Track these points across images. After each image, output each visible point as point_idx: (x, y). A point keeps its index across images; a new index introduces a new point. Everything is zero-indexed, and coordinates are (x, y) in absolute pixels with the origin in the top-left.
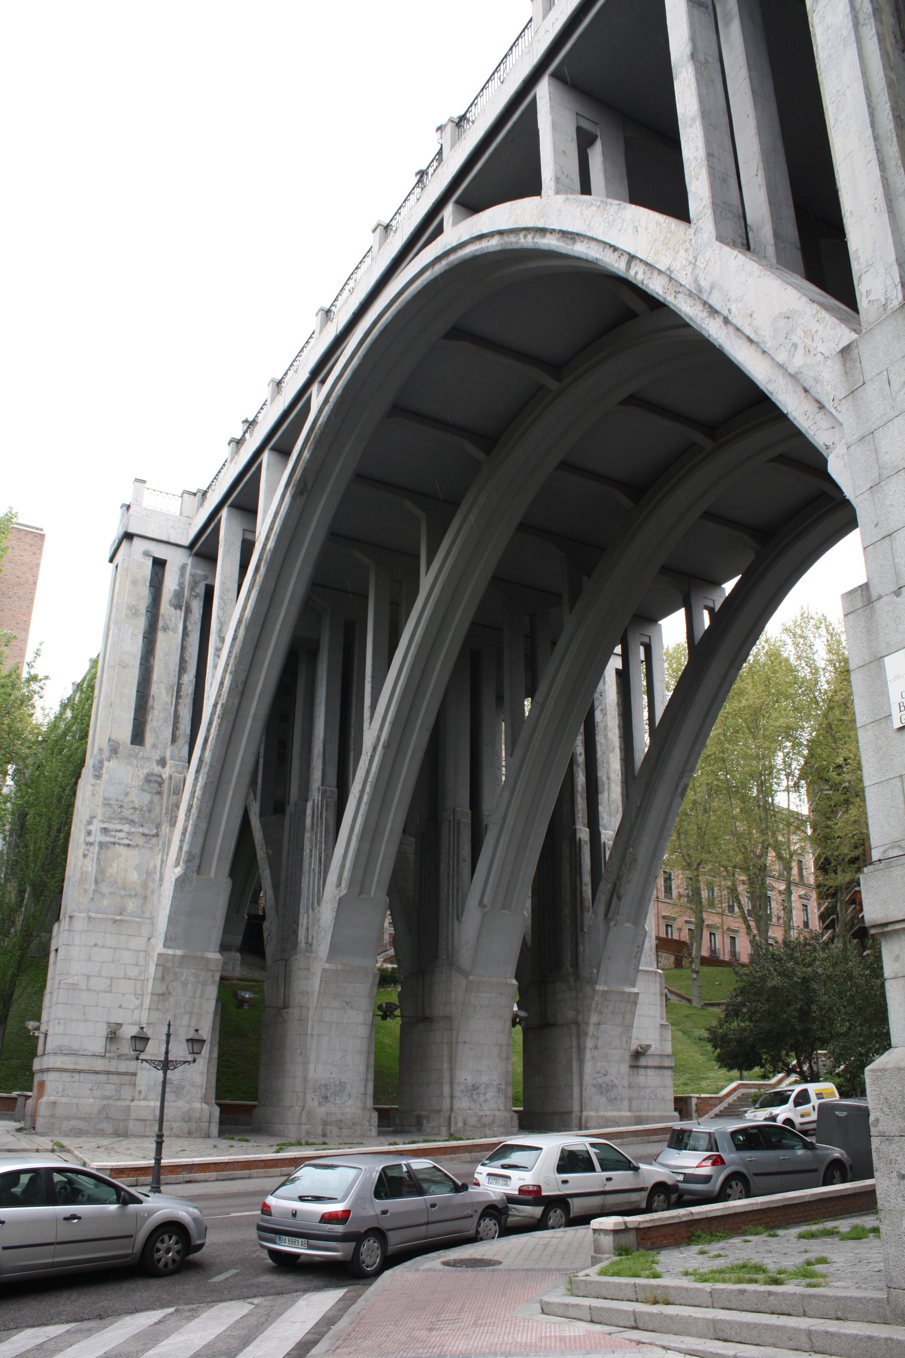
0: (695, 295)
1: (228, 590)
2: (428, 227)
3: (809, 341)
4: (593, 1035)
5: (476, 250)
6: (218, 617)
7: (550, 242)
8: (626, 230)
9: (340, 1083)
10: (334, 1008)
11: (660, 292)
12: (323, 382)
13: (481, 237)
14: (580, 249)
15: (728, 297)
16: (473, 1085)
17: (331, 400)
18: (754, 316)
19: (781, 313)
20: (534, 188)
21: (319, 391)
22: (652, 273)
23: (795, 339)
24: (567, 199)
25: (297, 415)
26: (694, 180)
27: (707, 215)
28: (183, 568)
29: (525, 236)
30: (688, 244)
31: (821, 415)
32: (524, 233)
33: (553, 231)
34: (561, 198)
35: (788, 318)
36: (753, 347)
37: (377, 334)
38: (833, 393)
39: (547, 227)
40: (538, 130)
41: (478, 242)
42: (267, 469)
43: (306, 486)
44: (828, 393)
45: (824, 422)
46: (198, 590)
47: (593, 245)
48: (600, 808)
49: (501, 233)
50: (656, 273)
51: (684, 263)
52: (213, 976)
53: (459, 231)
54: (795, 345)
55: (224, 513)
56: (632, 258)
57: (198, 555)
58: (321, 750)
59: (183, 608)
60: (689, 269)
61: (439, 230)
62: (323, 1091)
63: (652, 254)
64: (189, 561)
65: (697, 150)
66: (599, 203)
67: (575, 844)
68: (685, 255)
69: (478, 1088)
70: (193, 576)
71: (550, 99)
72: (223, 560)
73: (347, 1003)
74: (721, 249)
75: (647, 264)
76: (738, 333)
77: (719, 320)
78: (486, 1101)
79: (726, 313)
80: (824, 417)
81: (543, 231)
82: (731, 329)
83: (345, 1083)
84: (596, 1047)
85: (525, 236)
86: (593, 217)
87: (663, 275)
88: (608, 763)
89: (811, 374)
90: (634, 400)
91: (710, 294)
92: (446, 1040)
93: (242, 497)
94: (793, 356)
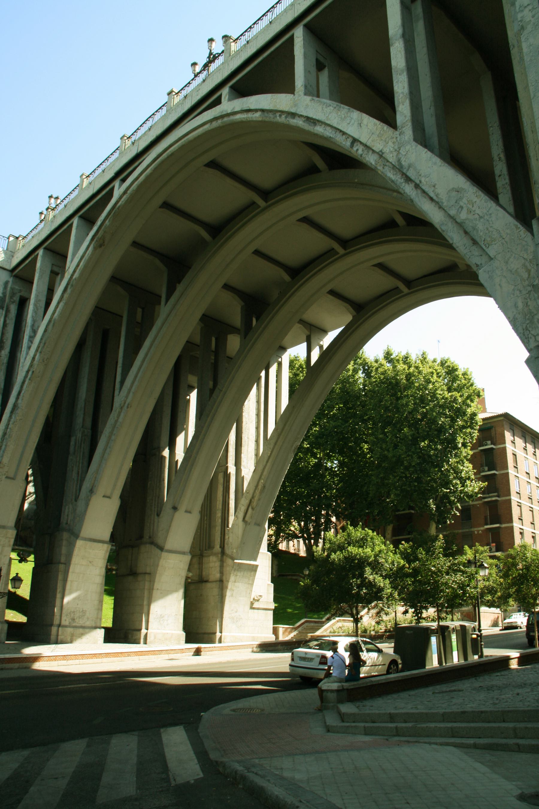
0: (399, 168)
1: (40, 301)
2: (210, 99)
3: (470, 206)
4: (231, 589)
5: (244, 118)
6: (33, 316)
7: (299, 122)
8: (353, 124)
9: (83, 611)
10: (82, 565)
11: (373, 163)
12: (123, 180)
13: (249, 111)
14: (319, 129)
15: (420, 174)
16: (161, 615)
17: (129, 192)
18: (436, 187)
19: (453, 188)
20: (290, 89)
21: (120, 186)
22: (368, 152)
23: (461, 204)
24: (313, 99)
25: (101, 199)
26: (401, 104)
27: (408, 126)
28: (6, 283)
29: (280, 116)
30: (394, 140)
31: (474, 247)
32: (279, 113)
33: (301, 116)
34: (308, 98)
35: (458, 192)
36: (434, 204)
37: (166, 157)
38: (484, 237)
39: (298, 113)
40: (294, 56)
41: (245, 113)
42: (77, 229)
43: (104, 242)
44: (481, 236)
45: (476, 251)
46: (15, 299)
47: (328, 128)
48: (242, 455)
49: (263, 111)
50: (371, 152)
51: (392, 149)
52: (9, 541)
53: (229, 105)
54: (462, 207)
55: (41, 252)
56: (355, 141)
57: (16, 276)
58: (83, 405)
59: (5, 309)
60: (395, 154)
61: (218, 102)
62: (72, 615)
63: (370, 141)
64: (11, 280)
65: (404, 88)
66: (335, 106)
67: (227, 477)
68: (393, 146)
69: (163, 617)
70: (12, 289)
71: (304, 39)
72: (38, 282)
73: (90, 562)
74: (416, 146)
75: (366, 146)
76: (424, 195)
77: (412, 185)
78: (168, 624)
79: (418, 182)
80: (476, 249)
81: (293, 115)
82: (419, 191)
83: (86, 611)
84: (232, 595)
85: (280, 116)
86: (330, 113)
87: (375, 154)
88: (249, 429)
89: (471, 224)
90: (306, 220)
91: (408, 170)
92: (146, 587)
93: (54, 244)
94: (460, 213)
